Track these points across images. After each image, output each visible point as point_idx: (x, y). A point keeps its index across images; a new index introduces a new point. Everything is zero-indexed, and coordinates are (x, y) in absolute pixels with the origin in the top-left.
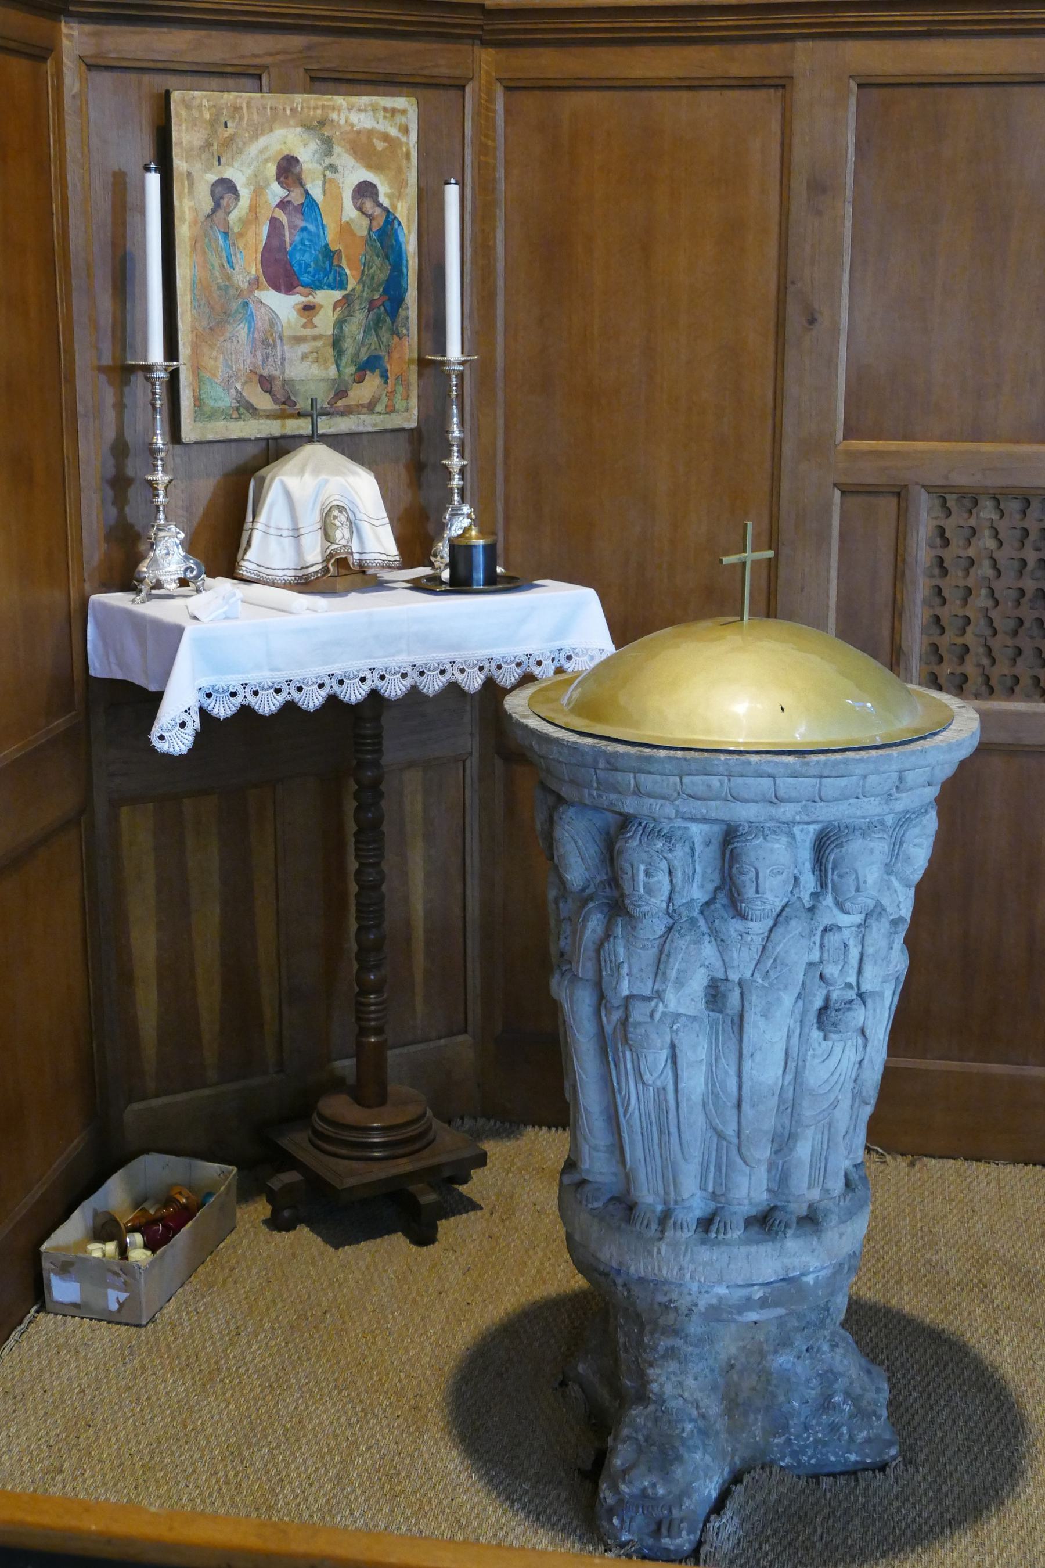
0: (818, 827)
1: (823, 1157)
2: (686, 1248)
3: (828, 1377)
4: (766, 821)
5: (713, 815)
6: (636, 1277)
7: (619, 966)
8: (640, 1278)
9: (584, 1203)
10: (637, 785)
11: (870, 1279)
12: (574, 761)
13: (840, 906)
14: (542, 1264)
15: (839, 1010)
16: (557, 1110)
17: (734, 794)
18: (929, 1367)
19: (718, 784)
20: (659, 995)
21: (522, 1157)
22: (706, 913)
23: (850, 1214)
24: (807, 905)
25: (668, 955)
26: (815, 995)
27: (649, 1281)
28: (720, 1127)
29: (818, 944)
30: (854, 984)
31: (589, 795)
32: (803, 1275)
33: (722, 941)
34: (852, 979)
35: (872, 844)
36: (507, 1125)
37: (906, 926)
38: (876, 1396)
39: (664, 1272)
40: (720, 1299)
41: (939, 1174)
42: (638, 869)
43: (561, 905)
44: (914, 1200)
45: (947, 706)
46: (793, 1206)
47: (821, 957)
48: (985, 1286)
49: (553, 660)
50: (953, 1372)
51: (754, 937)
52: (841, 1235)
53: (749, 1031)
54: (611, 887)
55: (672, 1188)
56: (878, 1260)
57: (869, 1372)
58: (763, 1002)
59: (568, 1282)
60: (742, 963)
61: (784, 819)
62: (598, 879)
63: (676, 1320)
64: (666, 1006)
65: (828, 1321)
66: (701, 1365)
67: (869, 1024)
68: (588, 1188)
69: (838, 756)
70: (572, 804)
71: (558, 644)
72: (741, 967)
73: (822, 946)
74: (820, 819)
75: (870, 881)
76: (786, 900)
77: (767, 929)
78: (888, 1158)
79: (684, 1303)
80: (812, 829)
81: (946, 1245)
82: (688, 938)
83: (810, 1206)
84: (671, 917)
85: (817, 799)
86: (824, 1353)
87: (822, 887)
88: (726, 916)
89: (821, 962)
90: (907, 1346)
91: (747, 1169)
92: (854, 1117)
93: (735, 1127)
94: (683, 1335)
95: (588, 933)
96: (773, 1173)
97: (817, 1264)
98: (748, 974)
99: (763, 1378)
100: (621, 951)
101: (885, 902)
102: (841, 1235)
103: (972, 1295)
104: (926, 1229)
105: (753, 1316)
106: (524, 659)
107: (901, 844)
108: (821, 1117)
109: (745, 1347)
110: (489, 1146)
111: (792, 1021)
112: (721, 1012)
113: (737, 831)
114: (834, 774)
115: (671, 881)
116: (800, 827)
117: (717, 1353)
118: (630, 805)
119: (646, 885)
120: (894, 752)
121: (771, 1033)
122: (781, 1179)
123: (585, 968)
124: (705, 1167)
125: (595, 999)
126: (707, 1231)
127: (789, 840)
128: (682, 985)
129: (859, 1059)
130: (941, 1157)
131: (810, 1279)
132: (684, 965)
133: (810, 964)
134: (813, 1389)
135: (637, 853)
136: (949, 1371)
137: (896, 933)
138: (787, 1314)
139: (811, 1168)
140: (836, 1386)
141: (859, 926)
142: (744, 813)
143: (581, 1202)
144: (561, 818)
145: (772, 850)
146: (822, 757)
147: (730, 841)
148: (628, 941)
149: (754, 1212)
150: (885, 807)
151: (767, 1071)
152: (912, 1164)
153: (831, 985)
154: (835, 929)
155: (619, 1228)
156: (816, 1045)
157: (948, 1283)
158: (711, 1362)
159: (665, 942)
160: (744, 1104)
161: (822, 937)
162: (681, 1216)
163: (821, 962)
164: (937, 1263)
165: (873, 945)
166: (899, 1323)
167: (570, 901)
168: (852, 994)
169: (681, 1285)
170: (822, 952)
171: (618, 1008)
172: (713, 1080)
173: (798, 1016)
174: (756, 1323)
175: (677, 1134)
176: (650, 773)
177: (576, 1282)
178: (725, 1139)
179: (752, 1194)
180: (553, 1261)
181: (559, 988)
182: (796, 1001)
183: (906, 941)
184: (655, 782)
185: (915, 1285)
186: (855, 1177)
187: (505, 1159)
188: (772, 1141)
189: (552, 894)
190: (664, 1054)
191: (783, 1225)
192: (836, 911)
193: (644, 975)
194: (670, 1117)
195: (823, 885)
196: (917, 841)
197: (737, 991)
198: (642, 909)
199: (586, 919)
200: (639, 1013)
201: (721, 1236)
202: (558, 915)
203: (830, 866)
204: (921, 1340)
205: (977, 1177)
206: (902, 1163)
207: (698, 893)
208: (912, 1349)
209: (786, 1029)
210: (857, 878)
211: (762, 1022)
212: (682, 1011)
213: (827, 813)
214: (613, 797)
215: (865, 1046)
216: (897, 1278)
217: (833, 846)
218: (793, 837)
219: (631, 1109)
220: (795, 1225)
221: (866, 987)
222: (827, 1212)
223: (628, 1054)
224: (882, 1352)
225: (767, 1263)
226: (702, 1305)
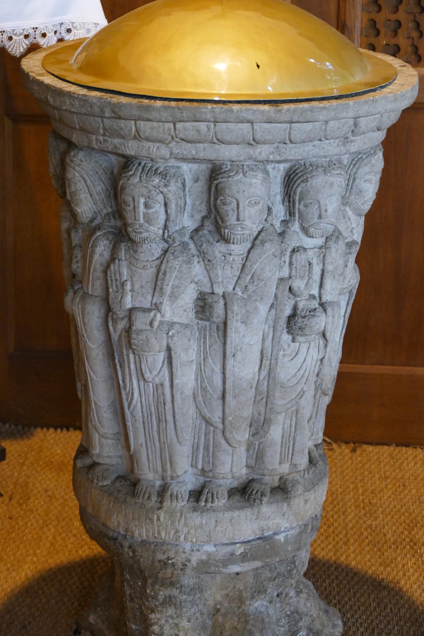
0: (287, 165)
1: (291, 439)
2: (181, 515)
3: (295, 616)
4: (245, 160)
5: (202, 155)
6: (139, 540)
7: (123, 284)
8: (142, 541)
9: (95, 481)
10: (137, 131)
11: (323, 542)
12: (83, 111)
13: (305, 231)
14: (54, 538)
15: (305, 317)
16: (66, 407)
17: (220, 137)
18: (372, 608)
19: (206, 129)
20: (157, 307)
21: (33, 453)
22: (194, 238)
23: (313, 485)
24: (279, 231)
25: (165, 274)
26: (285, 305)
27: (150, 543)
28: (208, 415)
29: (287, 263)
30: (317, 295)
31: (97, 140)
32: (275, 534)
33: (209, 261)
34: (315, 292)
35: (332, 179)
36: (20, 427)
37: (358, 248)
38: (332, 631)
39: (163, 534)
40: (209, 555)
41: (375, 458)
42: (139, 203)
43: (73, 235)
44: (357, 479)
45: (390, 65)
46: (267, 479)
47: (290, 274)
48: (415, 544)
49: (55, 32)
50: (392, 611)
51: (236, 258)
52: (306, 501)
53: (232, 335)
54: (115, 218)
55: (168, 464)
56: (329, 527)
57: (327, 612)
58: (243, 311)
59: (77, 551)
60: (226, 279)
61: (260, 158)
62: (105, 211)
63: (173, 574)
64: (163, 316)
65: (295, 571)
66: (193, 610)
67: (329, 328)
68: (98, 469)
69: (305, 105)
70: (81, 149)
71: (58, 19)
72: (225, 282)
73: (291, 264)
74: (290, 158)
75: (330, 210)
76: (262, 226)
77: (246, 250)
78: (335, 446)
79: (179, 559)
80: (283, 167)
81: (382, 513)
82: (181, 259)
83: (281, 479)
84: (167, 242)
85: (288, 141)
86: (291, 598)
87: (290, 215)
88: (211, 240)
89: (290, 278)
90: (354, 593)
91: (231, 449)
92: (316, 405)
93: (221, 415)
94: (178, 586)
95: (96, 257)
96: (251, 452)
97: (287, 525)
98: (231, 288)
99: (242, 619)
100: (125, 271)
101: (342, 228)
102: (306, 501)
103: (405, 551)
104: (366, 501)
105: (235, 568)
106: (31, 31)
107: (354, 180)
108: (289, 405)
109: (228, 595)
110: (6, 444)
111: (267, 327)
112: (208, 320)
113: (221, 168)
114: (301, 119)
115: (166, 211)
116: (273, 166)
117: (206, 599)
118: (131, 148)
119: (145, 215)
120: (351, 102)
121: (249, 336)
122: (257, 456)
123: (95, 287)
124: (195, 449)
125: (103, 311)
126: (198, 500)
127: (264, 175)
128: (176, 298)
129: (320, 357)
130: (377, 444)
131: (281, 537)
132: (177, 282)
133: (281, 280)
134: (282, 627)
135: (137, 186)
136: (388, 610)
137: (350, 253)
138: (262, 567)
139: (282, 447)
140: (301, 624)
141: (320, 248)
142: (227, 153)
143: (92, 481)
144: (72, 161)
145: (250, 184)
146: (292, 106)
147: (215, 178)
148: (130, 263)
149: (235, 484)
150: (342, 148)
151: (245, 368)
152: (354, 450)
153: (298, 296)
154: (302, 251)
155: (125, 501)
156: (286, 346)
157: (386, 543)
158: (200, 607)
159: (162, 262)
160: (227, 396)
161: (291, 257)
162: (176, 489)
163: (290, 278)
164: (376, 527)
165: (332, 263)
166: (347, 575)
167: (80, 231)
168: (315, 304)
169: (177, 545)
170: (291, 269)
171: (122, 319)
172: (201, 375)
173: (271, 323)
174: (238, 574)
175: (172, 422)
176: (149, 120)
177: (84, 552)
178: (211, 425)
179: (234, 469)
180: (63, 535)
181: (72, 304)
182: (270, 310)
183: (357, 261)
184: (152, 128)
185: (360, 545)
186: (316, 454)
187: (20, 455)
188: (250, 426)
189: (65, 225)
190: (162, 356)
191: (259, 493)
192: (302, 235)
193: (144, 291)
194: (167, 408)
195: (291, 214)
196: (368, 177)
197: (222, 302)
198: (142, 235)
199: (94, 246)
200: (140, 322)
201: (209, 505)
202: (70, 244)
203: (297, 198)
204: (365, 587)
205: (407, 459)
206: (346, 449)
207: (188, 222)
208: (358, 595)
209: (261, 333)
210: (319, 207)
211: (242, 328)
212: (176, 320)
213: (295, 153)
214: (116, 141)
215: (326, 346)
216: (345, 540)
217: (299, 181)
218: (267, 172)
219: (134, 402)
220: (269, 494)
221: (326, 298)
222: (295, 483)
223: (131, 356)
224: (335, 598)
225: (245, 525)
226: (194, 560)
